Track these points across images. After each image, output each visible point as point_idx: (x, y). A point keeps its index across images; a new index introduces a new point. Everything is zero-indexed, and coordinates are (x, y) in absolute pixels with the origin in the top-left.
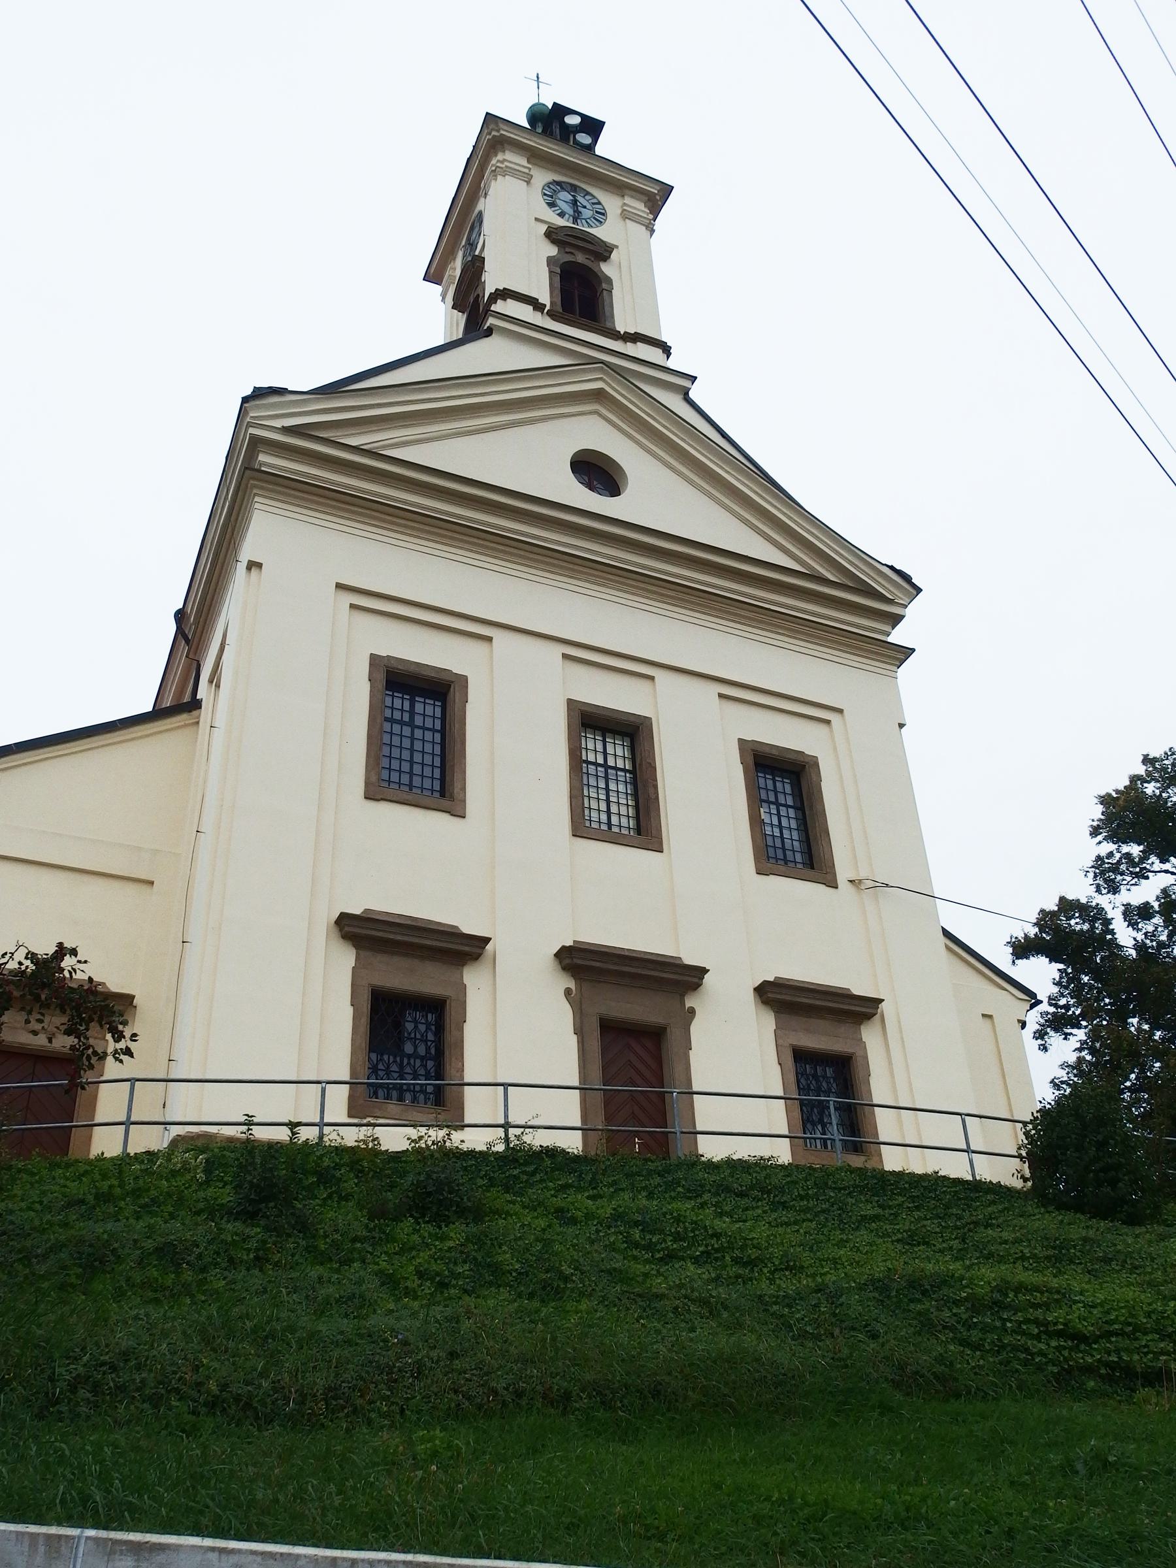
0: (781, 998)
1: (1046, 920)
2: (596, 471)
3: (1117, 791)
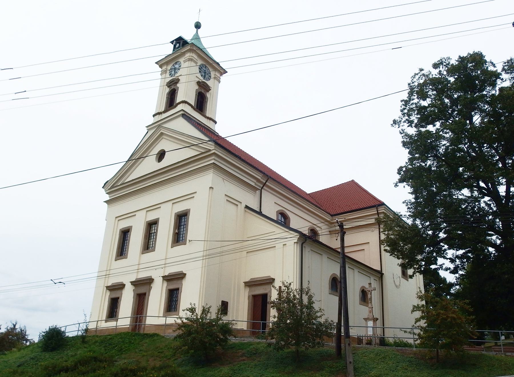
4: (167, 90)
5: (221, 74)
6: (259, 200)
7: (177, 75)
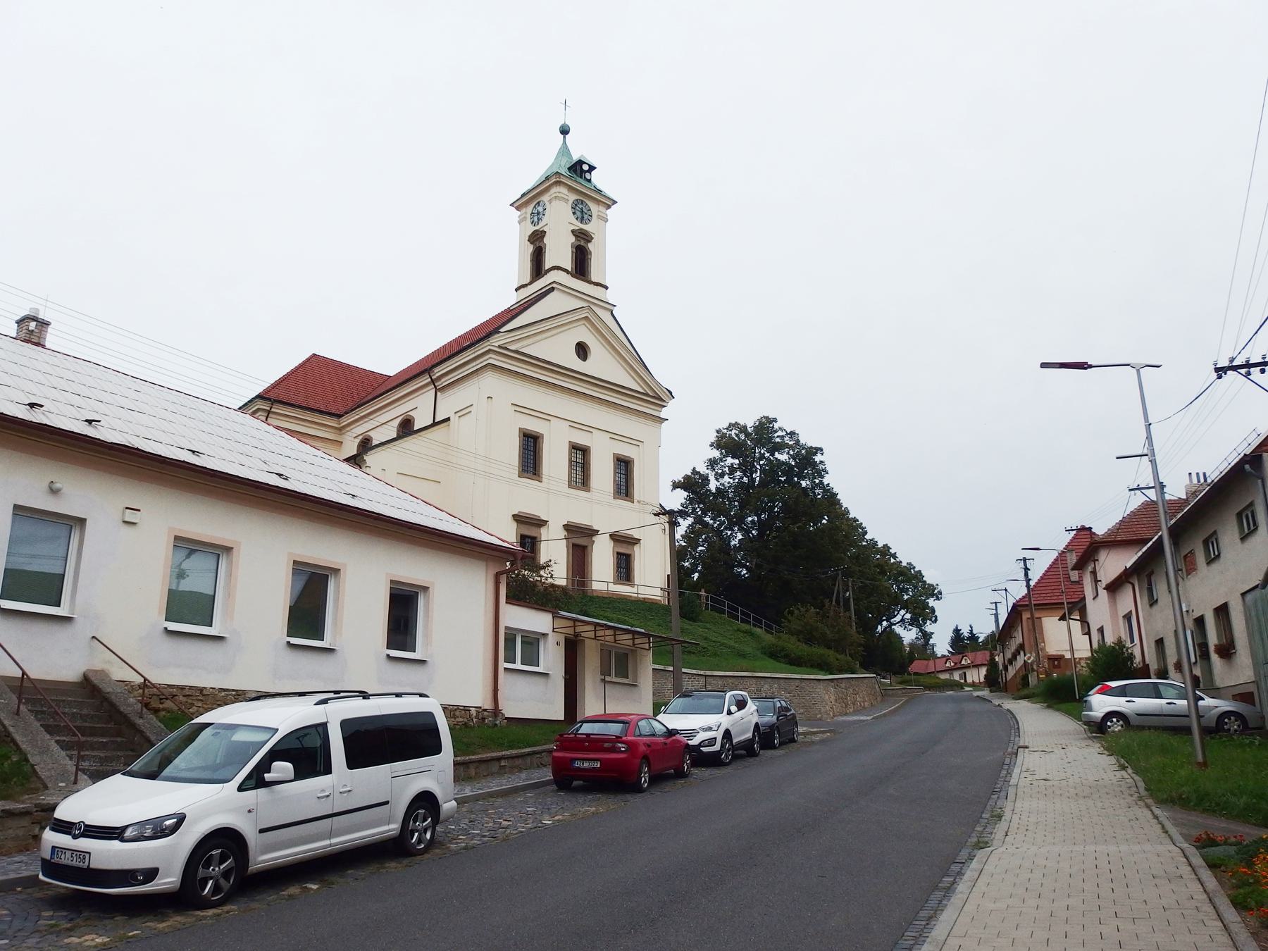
0: (616, 538)
1: (687, 478)
2: (582, 350)
3: (682, 505)
4: (531, 248)
5: (609, 207)
6: (491, 615)
7: (541, 224)
